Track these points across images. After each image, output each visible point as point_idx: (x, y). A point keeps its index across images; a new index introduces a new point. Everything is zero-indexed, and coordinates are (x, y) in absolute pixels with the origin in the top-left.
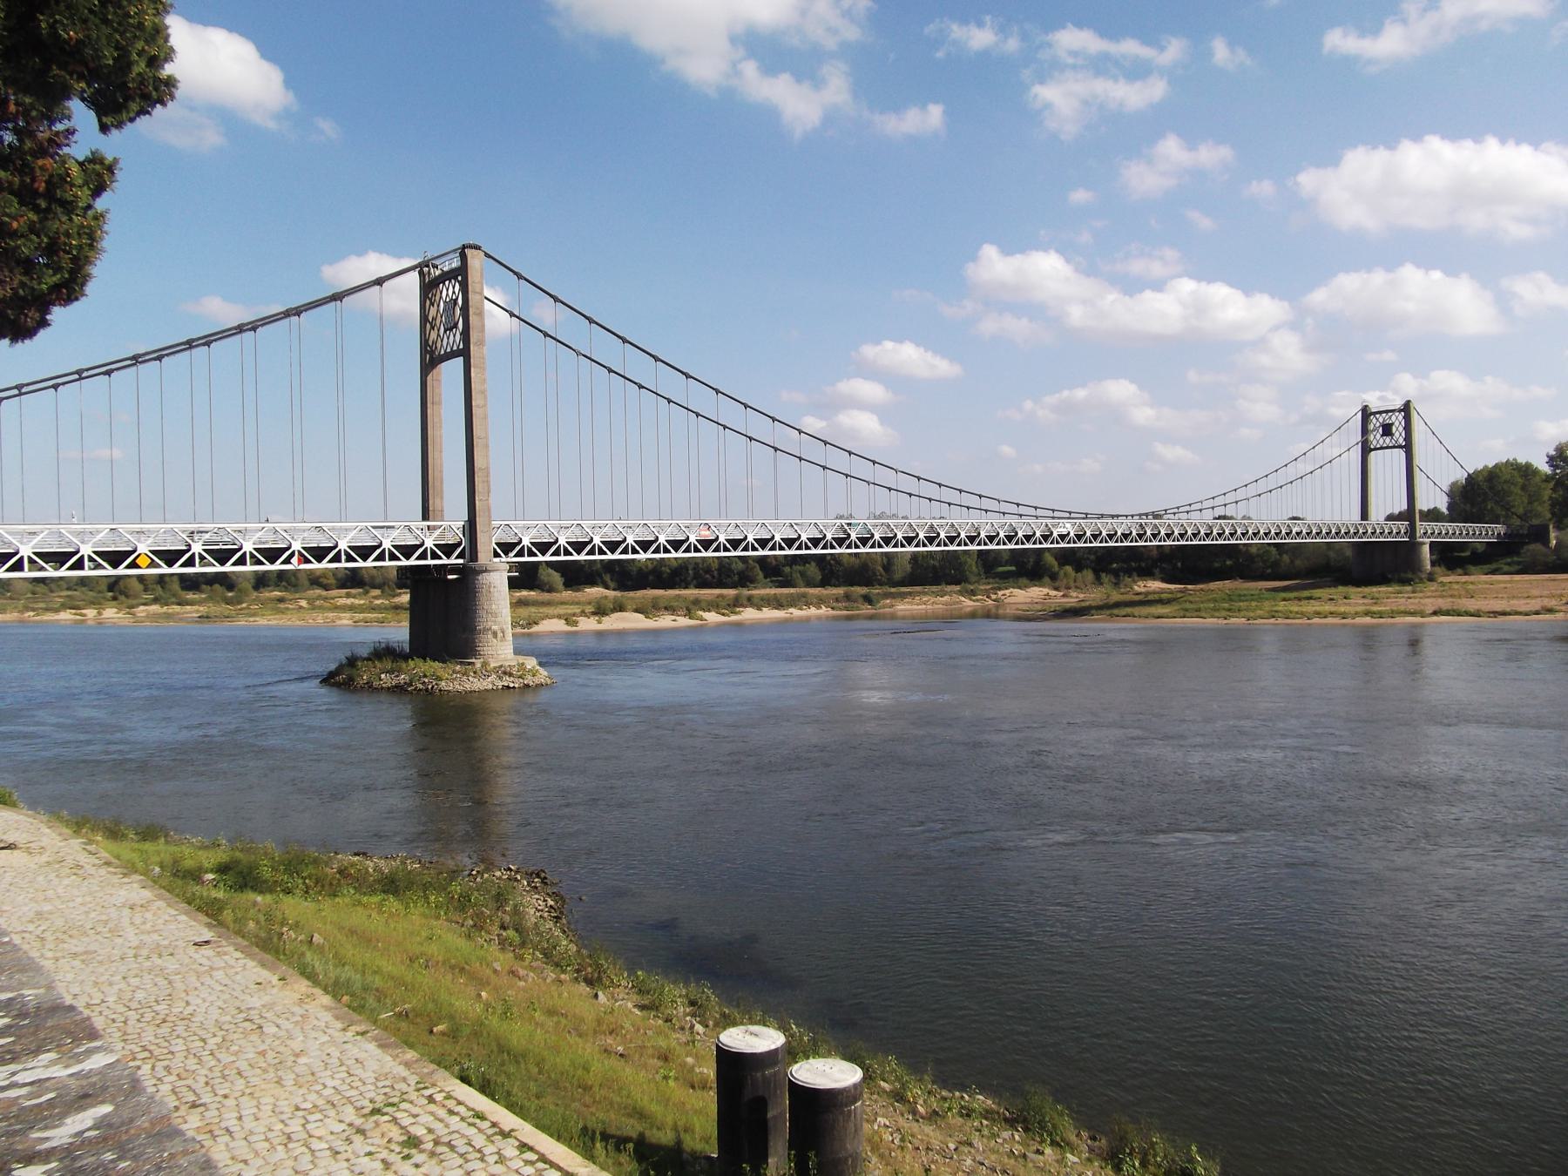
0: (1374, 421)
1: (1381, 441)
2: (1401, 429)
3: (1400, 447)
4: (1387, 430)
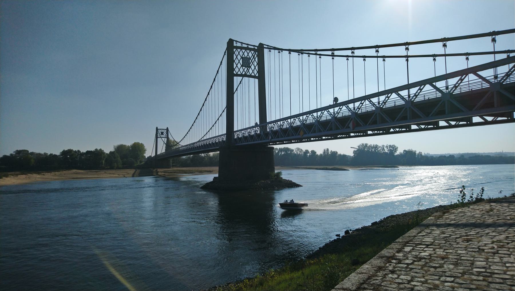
1: (164, 131)
2: (237, 61)
3: (254, 77)
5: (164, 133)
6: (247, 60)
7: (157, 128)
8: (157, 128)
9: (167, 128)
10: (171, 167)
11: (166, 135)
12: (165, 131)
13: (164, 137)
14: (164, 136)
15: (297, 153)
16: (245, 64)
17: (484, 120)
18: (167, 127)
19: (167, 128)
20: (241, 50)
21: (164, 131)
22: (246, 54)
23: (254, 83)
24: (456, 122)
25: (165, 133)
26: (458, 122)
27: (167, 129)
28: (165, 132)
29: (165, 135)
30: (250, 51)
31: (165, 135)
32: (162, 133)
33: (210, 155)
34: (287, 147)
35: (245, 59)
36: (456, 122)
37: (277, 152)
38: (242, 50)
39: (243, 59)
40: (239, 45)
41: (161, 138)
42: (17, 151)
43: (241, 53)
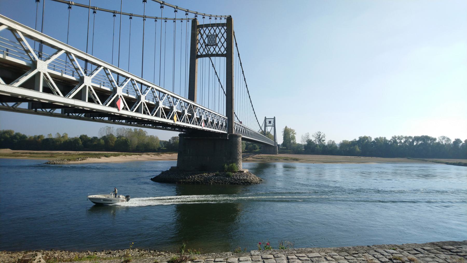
0: (223, 49)
1: (271, 120)
2: (223, 40)
3: (222, 55)
4: (270, 122)
5: (271, 122)
6: (213, 37)
7: (265, 117)
8: (265, 117)
9: (275, 117)
10: (278, 154)
11: (273, 124)
12: (273, 120)
13: (271, 126)
14: (271, 125)
15: (442, 142)
16: (211, 42)
17: (95, 204)
18: (274, 117)
19: (275, 117)
20: (218, 27)
21: (271, 120)
22: (212, 31)
23: (221, 62)
24: (53, 112)
25: (272, 122)
26: (52, 110)
27: (274, 118)
28: (272, 121)
29: (272, 124)
30: (222, 53)
31: (272, 124)
32: (270, 122)
33: (325, 143)
34: (426, 135)
35: (211, 37)
36: (53, 112)
37: (411, 140)
38: (219, 27)
39: (209, 38)
40: (207, 21)
41: (261, 128)
42: (173, 137)
43: (217, 49)
